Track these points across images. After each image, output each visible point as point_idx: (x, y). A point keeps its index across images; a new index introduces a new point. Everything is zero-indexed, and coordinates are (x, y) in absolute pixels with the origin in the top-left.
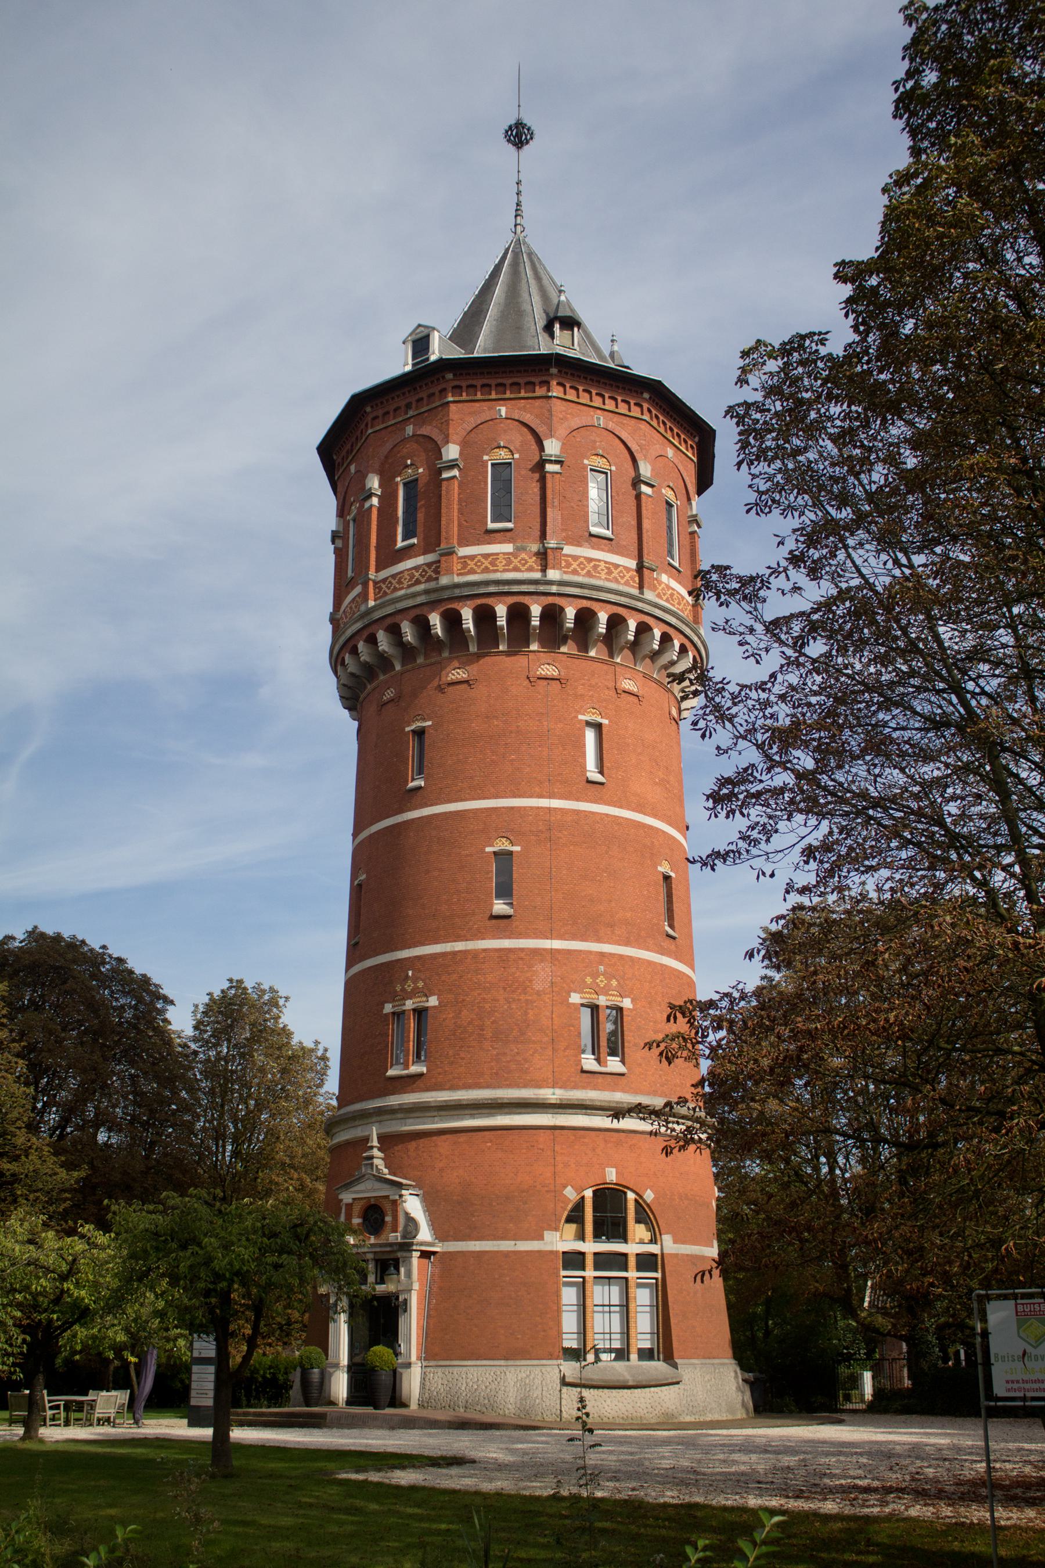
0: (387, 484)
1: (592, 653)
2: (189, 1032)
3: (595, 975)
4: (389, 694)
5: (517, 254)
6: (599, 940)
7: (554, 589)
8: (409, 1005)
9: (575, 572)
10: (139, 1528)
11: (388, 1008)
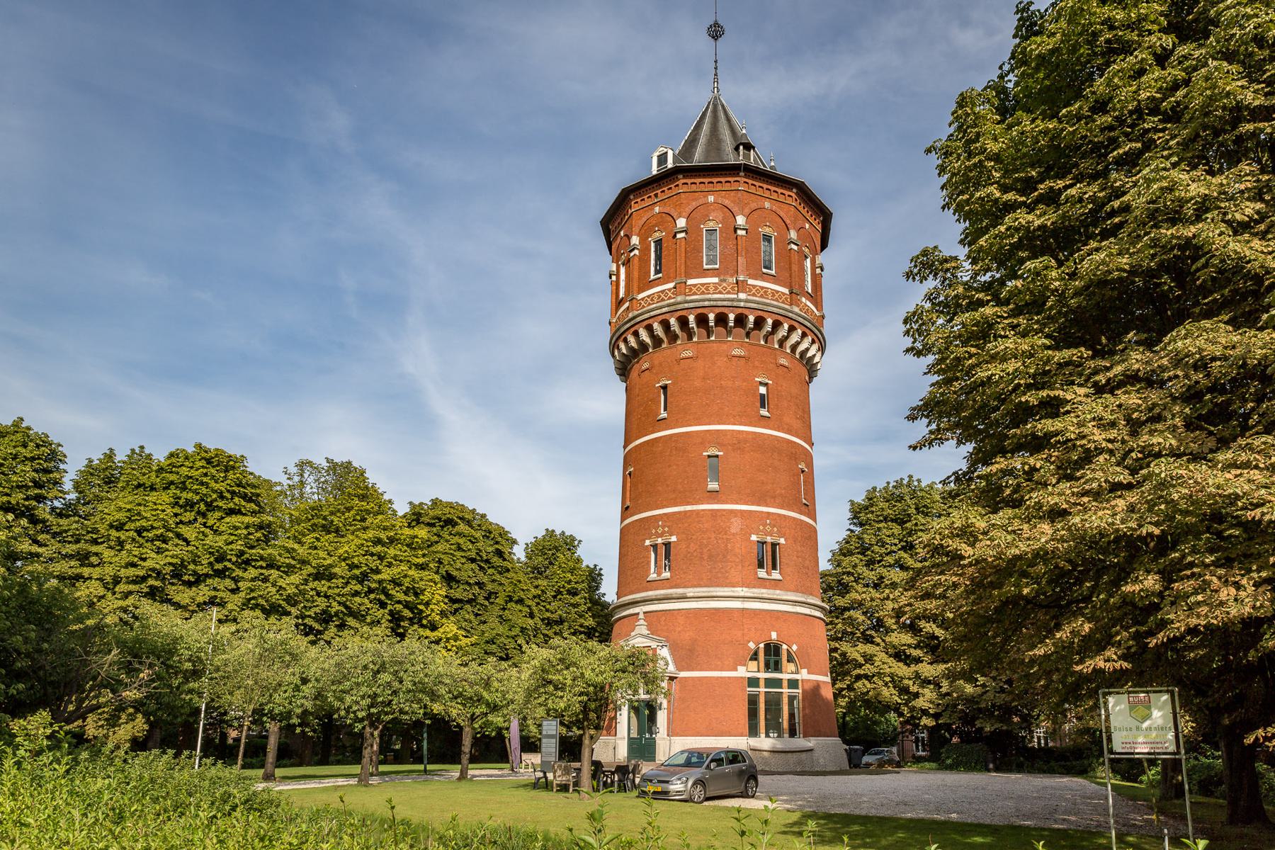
0: (643, 240)
1: (695, 339)
2: (523, 559)
3: (765, 525)
4: (646, 366)
5: (715, 106)
6: (767, 506)
7: (742, 304)
8: (660, 541)
9: (754, 295)
10: (1129, 666)
11: (648, 543)
